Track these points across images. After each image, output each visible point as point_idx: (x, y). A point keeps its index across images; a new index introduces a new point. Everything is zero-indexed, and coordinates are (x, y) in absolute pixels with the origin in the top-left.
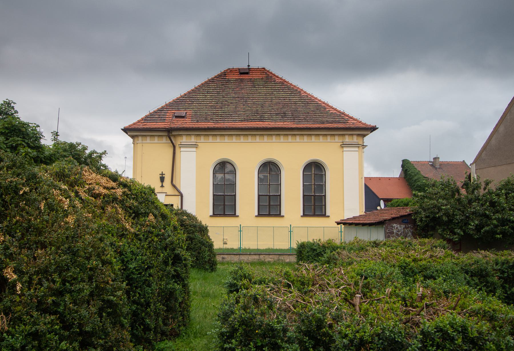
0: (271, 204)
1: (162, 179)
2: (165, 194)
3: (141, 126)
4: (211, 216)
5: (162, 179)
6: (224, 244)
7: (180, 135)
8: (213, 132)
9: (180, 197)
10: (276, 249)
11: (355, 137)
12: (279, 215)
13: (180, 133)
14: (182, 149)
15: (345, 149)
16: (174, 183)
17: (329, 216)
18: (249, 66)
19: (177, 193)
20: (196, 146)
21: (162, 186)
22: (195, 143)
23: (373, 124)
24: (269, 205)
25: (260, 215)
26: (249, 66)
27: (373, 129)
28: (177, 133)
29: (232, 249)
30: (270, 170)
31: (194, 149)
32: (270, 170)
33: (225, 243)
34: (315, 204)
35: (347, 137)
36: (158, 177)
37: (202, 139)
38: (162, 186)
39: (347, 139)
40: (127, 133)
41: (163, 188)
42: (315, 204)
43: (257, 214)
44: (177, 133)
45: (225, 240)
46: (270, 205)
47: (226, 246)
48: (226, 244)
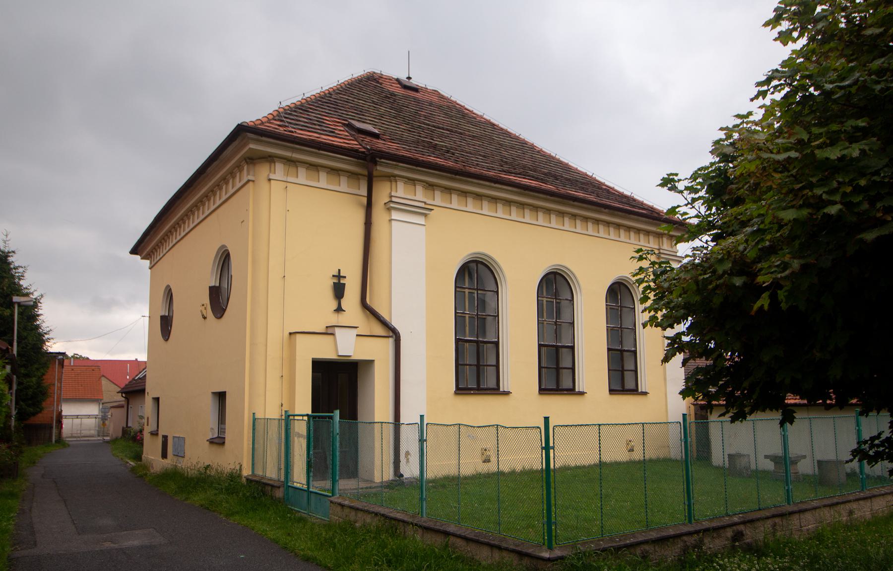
1: (339, 290)
2: (355, 332)
3: (274, 127)
5: (339, 290)
7: (270, 159)
8: (467, 183)
9: (391, 341)
10: (513, 473)
11: (419, 189)
13: (397, 172)
15: (395, 215)
17: (645, 394)
19: (379, 330)
20: (424, 211)
21: (339, 309)
22: (422, 205)
28: (288, 154)
30: (555, 287)
31: (421, 220)
35: (401, 185)
36: (330, 282)
37: (438, 198)
38: (339, 309)
44: (288, 154)
47: (492, 467)
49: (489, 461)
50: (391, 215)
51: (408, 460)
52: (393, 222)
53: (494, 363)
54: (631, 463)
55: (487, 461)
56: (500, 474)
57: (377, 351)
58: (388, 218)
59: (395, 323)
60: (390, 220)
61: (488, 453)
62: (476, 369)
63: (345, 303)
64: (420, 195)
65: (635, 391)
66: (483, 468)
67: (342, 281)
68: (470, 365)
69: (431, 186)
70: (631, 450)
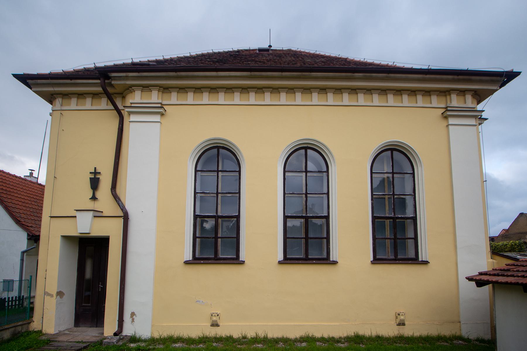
0: (311, 235)
1: (95, 183)
2: (91, 214)
4: (187, 263)
5: (95, 183)
6: (212, 325)
9: (121, 220)
12: (326, 260)
14: (133, 118)
15: (451, 121)
16: (118, 191)
17: (426, 263)
18: (270, 46)
20: (160, 110)
21: (94, 198)
23: (507, 68)
24: (307, 238)
25: (287, 260)
26: (270, 46)
27: (506, 77)
29: (387, 65)
30: (307, 160)
31: (157, 118)
32: (307, 160)
33: (215, 325)
34: (395, 235)
36: (88, 177)
37: (174, 98)
38: (94, 198)
39: (455, 101)
40: (31, 88)
41: (96, 202)
42: (395, 235)
43: (281, 257)
45: (214, 318)
46: (307, 241)
48: (217, 325)
49: (404, 324)
50: (448, 122)
51: (133, 320)
52: (450, 127)
53: (413, 236)
54: (401, 339)
55: (215, 325)
56: (229, 339)
57: (111, 229)
58: (447, 124)
59: (128, 207)
60: (448, 126)
61: (402, 317)
62: (216, 240)
63: (98, 195)
64: (155, 97)
65: (415, 260)
66: (212, 332)
67: (98, 176)
68: (390, 239)
69: (165, 90)
70: (402, 324)
